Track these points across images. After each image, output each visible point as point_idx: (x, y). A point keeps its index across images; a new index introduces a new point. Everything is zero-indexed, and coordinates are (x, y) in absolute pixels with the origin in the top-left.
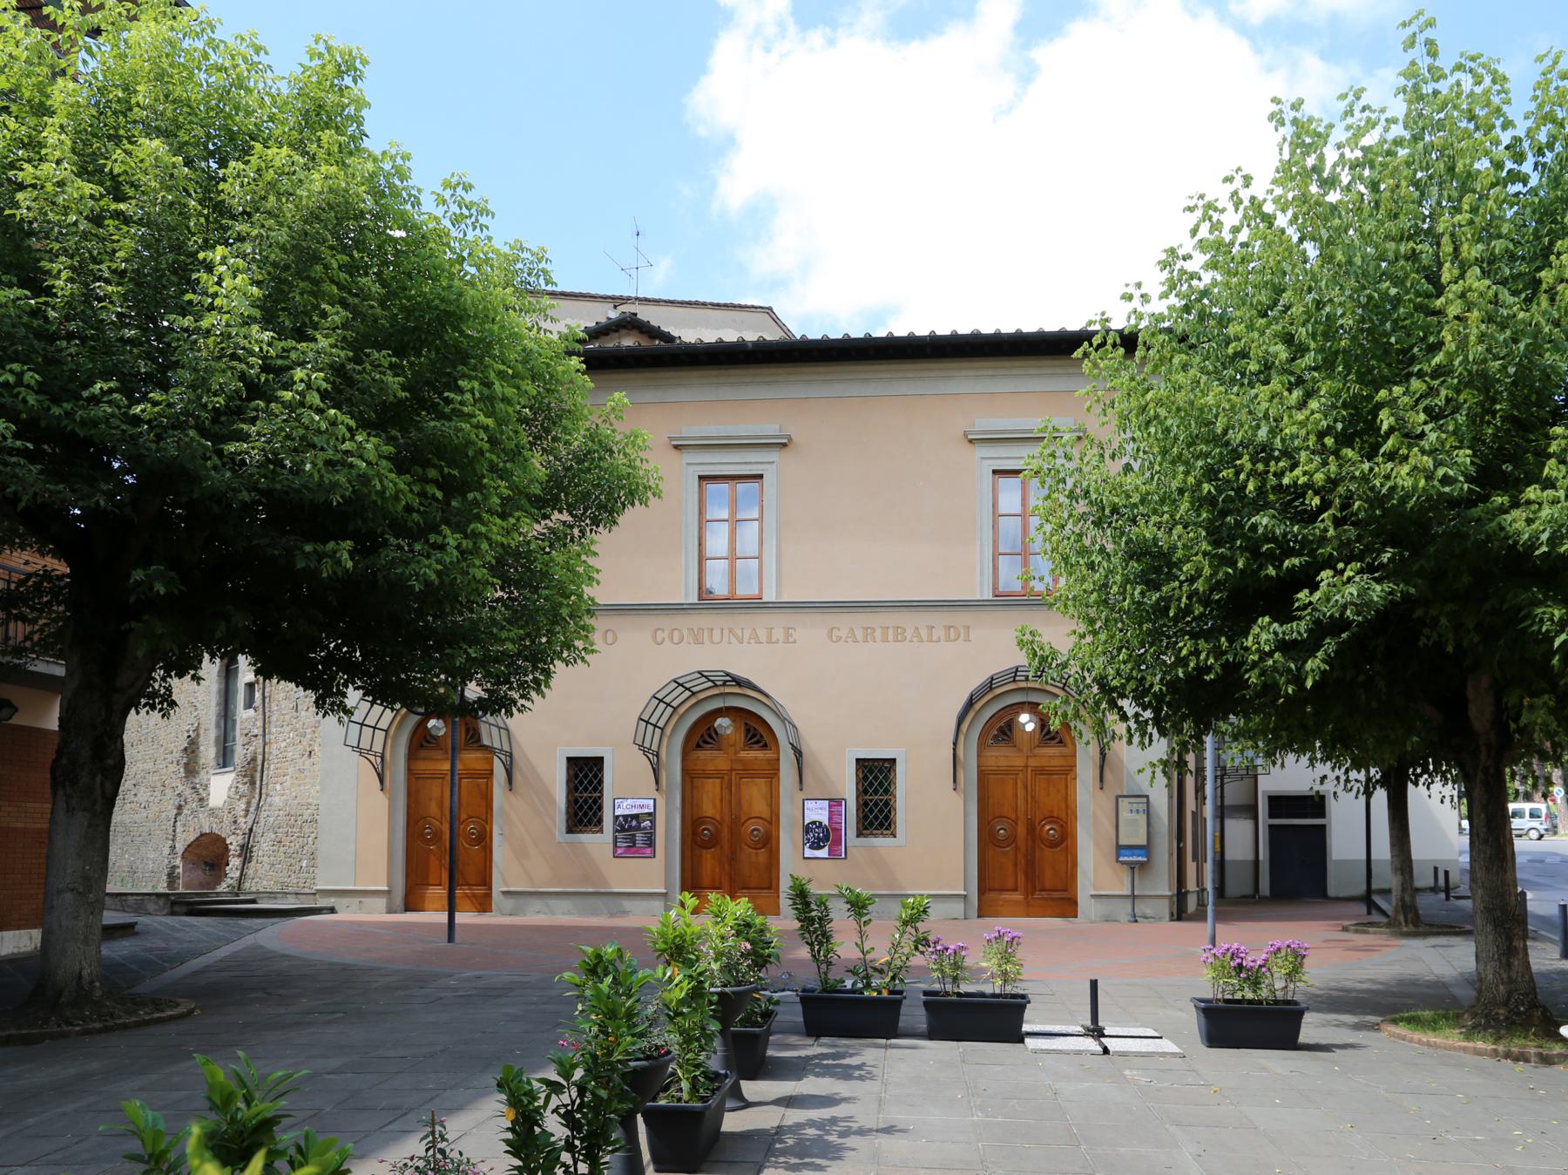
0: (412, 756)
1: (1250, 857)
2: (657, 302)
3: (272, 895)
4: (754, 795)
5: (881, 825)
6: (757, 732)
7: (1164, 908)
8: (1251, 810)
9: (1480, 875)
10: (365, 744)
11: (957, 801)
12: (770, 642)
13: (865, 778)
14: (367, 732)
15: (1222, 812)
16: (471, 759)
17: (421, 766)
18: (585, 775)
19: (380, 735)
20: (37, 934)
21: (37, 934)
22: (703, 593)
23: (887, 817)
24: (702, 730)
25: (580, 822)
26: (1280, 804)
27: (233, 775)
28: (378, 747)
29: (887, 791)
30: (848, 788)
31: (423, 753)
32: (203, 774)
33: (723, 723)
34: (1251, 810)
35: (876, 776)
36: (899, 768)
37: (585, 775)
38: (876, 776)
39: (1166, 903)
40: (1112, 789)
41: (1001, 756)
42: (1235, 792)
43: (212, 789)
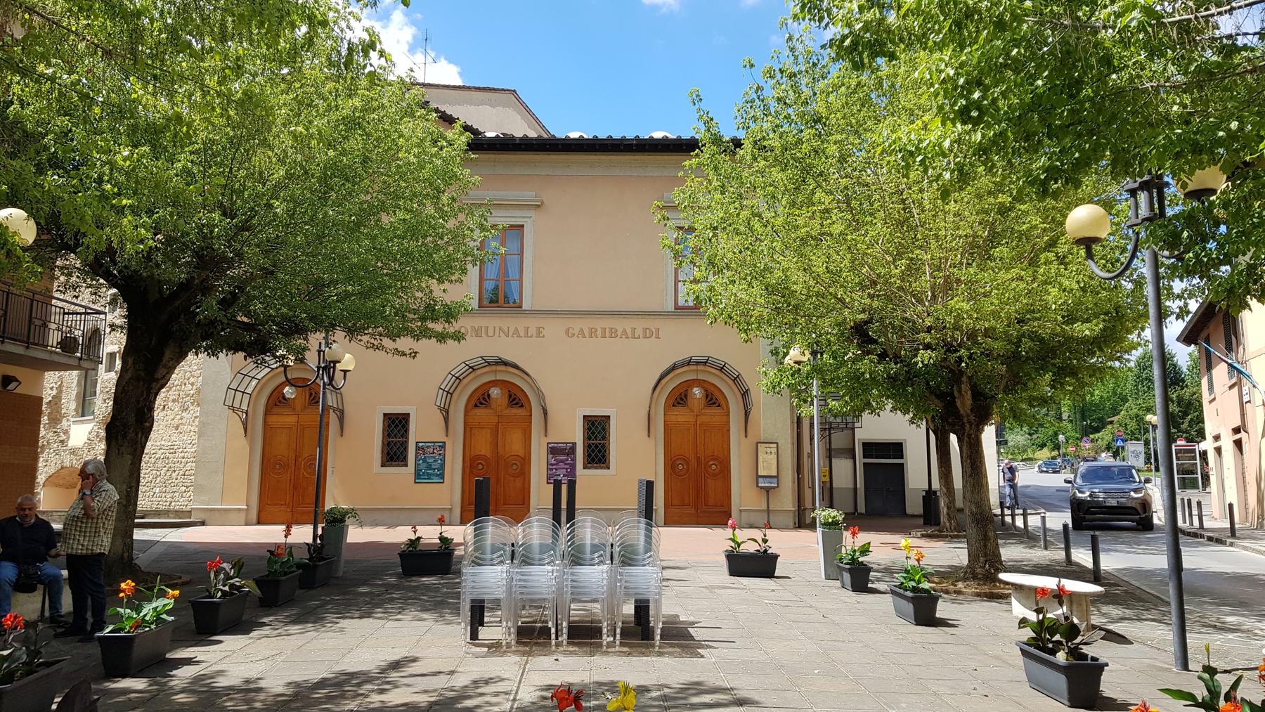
0: (267, 412)
1: (851, 486)
2: (438, 86)
3: (158, 513)
4: (514, 444)
5: (600, 461)
6: (516, 399)
7: (790, 520)
8: (851, 453)
9: (968, 494)
10: (236, 405)
11: (241, 444)
12: (527, 336)
13: (589, 429)
14: (239, 395)
15: (830, 454)
16: (311, 417)
17: (273, 419)
18: (396, 425)
19: (246, 397)
20: (863, 511)
21: (863, 511)
22: (677, 307)
23: (604, 456)
24: (480, 392)
25: (593, 460)
26: (872, 448)
27: (89, 426)
28: (244, 407)
29: (604, 438)
30: (576, 435)
31: (276, 410)
32: (64, 423)
33: (495, 392)
34: (851, 453)
35: (596, 428)
36: (613, 422)
37: (396, 425)
38: (596, 428)
39: (791, 515)
40: (752, 439)
41: (681, 416)
42: (839, 440)
43: (72, 433)
